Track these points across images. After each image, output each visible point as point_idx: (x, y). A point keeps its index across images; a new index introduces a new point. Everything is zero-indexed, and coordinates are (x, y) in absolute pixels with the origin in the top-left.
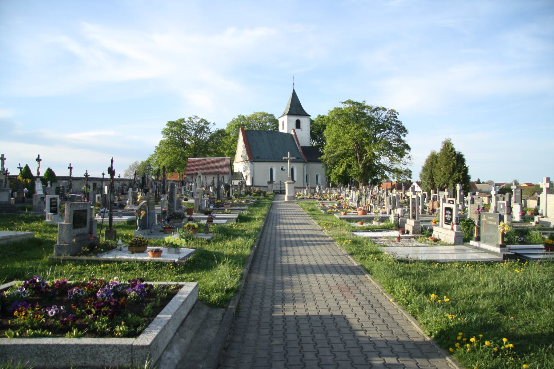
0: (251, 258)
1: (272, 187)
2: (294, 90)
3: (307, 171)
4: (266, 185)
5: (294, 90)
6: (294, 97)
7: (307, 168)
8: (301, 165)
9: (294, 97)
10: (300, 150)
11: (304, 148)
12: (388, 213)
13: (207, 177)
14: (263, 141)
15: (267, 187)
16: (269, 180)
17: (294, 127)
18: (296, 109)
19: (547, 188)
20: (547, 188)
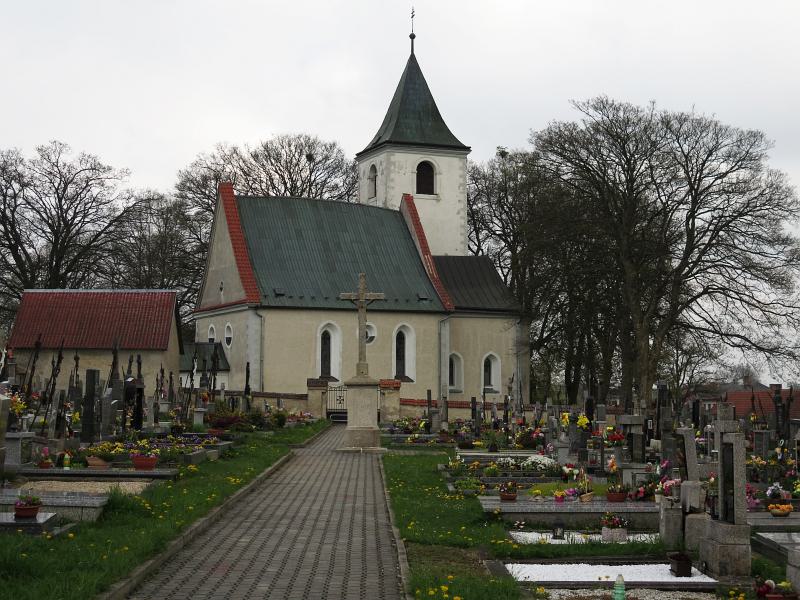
0: (405, 207)
1: (324, 400)
2: (413, 58)
3: (454, 344)
4: (304, 390)
5: (413, 58)
6: (413, 77)
7: (452, 333)
8: (430, 323)
9: (413, 77)
10: (430, 269)
11: (444, 263)
12: (452, 388)
13: (64, 355)
14: (299, 233)
15: (304, 397)
16: (317, 374)
17: (412, 189)
18: (414, 118)
19: (780, 386)
20: (780, 386)
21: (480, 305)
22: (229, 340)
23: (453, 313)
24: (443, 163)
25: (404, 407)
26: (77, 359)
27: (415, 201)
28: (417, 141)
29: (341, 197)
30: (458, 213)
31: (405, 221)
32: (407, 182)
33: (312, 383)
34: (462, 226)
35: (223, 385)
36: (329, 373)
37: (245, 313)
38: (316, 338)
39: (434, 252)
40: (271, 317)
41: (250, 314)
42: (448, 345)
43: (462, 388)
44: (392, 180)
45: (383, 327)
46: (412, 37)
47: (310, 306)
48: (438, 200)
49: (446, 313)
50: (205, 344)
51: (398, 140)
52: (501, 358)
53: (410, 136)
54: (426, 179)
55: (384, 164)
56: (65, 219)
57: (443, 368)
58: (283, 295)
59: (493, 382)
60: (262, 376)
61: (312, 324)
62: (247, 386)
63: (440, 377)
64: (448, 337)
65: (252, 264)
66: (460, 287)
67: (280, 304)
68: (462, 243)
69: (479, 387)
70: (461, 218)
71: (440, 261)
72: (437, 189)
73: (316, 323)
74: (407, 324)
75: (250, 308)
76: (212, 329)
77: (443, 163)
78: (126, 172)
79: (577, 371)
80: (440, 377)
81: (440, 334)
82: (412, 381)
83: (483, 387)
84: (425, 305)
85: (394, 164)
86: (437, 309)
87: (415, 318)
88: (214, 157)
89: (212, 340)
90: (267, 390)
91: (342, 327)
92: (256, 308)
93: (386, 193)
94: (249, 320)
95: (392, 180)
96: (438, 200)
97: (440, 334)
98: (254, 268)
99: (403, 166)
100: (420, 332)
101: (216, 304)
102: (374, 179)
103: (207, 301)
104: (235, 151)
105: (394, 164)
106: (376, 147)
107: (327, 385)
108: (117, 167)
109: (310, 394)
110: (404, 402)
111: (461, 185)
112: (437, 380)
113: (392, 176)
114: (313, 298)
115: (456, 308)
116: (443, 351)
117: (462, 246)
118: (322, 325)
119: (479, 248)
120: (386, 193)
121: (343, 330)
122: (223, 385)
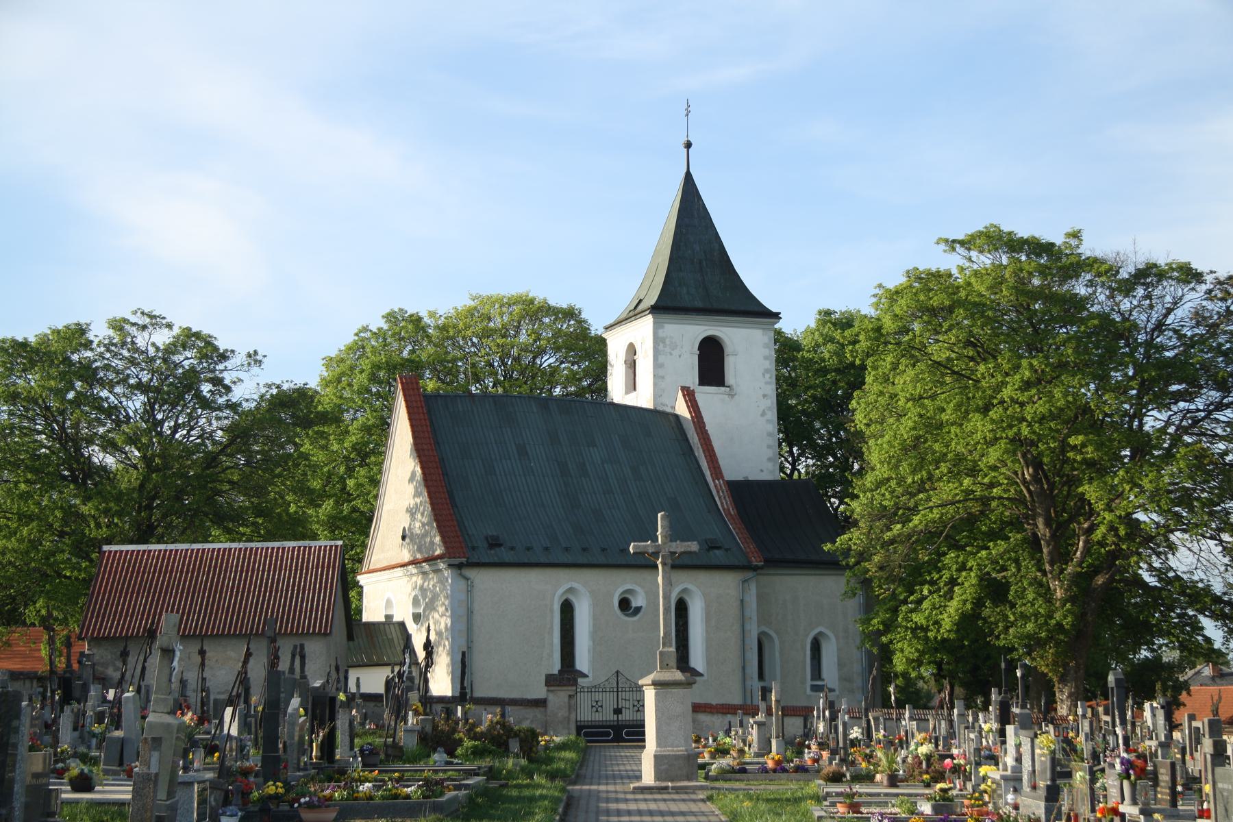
1: (572, 707)
3: (763, 618)
4: (540, 692)
5: (688, 177)
6: (692, 214)
7: (761, 598)
8: (726, 584)
9: (692, 214)
10: (723, 501)
11: (743, 491)
15: (540, 703)
16: (556, 667)
18: (699, 278)
23: (762, 568)
26: (202, 653)
27: (698, 397)
29: (581, 392)
30: (763, 414)
33: (551, 681)
34: (770, 434)
38: (552, 611)
39: (727, 478)
42: (755, 618)
46: (688, 145)
47: (542, 560)
48: (732, 396)
50: (378, 624)
52: (837, 638)
56: (160, 434)
57: (748, 655)
58: (500, 545)
59: (825, 674)
63: (744, 668)
64: (754, 606)
67: (496, 560)
68: (769, 459)
69: (803, 682)
70: (768, 421)
72: (730, 378)
74: (575, 585)
79: (292, 670)
80: (744, 668)
81: (742, 601)
82: (701, 675)
83: (809, 683)
85: (664, 343)
86: (737, 563)
87: (703, 577)
88: (764, 396)
91: (646, 593)
97: (742, 601)
100: (708, 595)
109: (551, 697)
112: (739, 675)
114: (547, 549)
115: (766, 561)
116: (747, 627)
117: (770, 465)
118: (561, 591)
119: (794, 469)
121: (590, 594)
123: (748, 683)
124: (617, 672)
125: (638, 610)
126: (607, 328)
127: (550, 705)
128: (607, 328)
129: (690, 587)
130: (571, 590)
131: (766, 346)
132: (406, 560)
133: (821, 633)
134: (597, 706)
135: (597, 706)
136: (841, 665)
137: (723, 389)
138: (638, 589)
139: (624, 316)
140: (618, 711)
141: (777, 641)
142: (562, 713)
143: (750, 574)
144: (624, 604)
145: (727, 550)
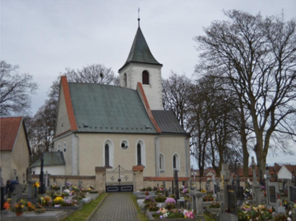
2: (139, 32)
4: (93, 174)
5: (139, 32)
6: (139, 36)
8: (151, 139)
9: (139, 36)
10: (150, 115)
12: (161, 170)
15: (93, 178)
21: (170, 131)
22: (65, 150)
24: (152, 71)
25: (145, 182)
28: (142, 61)
30: (159, 93)
31: (139, 94)
32: (139, 78)
33: (99, 170)
35: (47, 172)
36: (108, 164)
37: (70, 136)
40: (82, 137)
41: (73, 135)
43: (165, 170)
44: (133, 78)
45: (132, 141)
46: (139, 20)
48: (151, 87)
49: (158, 134)
51: (135, 60)
53: (139, 60)
54: (146, 77)
55: (130, 72)
60: (78, 167)
61: (99, 141)
62: (176, 172)
65: (75, 112)
66: (164, 124)
71: (154, 112)
73: (102, 140)
74: (109, 139)
75: (73, 132)
76: (65, 144)
77: (152, 71)
78: (17, 67)
81: (155, 145)
84: (149, 131)
87: (145, 137)
89: (59, 151)
90: (81, 174)
92: (75, 133)
93: (130, 84)
94: (73, 138)
95: (133, 78)
96: (151, 87)
97: (155, 145)
98: (75, 114)
99: (137, 72)
100: (147, 142)
101: (61, 133)
102: (125, 80)
103: (58, 133)
104: (73, 71)
105: (133, 71)
106: (127, 64)
107: (105, 171)
108: (13, 64)
110: (147, 179)
111: (159, 80)
112: (155, 166)
113: (133, 76)
116: (157, 152)
120: (130, 84)
121: (114, 142)
122: (47, 172)
123: (157, 169)
124: (119, 166)
125: (127, 147)
126: (125, 75)
127: (96, 178)
128: (125, 75)
129: (142, 140)
130: (108, 141)
131: (160, 102)
132: (263, 99)
133: (176, 154)
134: (112, 178)
135: (112, 178)
136: (181, 164)
137: (148, 85)
138: (127, 140)
139: (198, 161)
140: (119, 180)
141: (164, 157)
142: (101, 182)
143: (157, 136)
144: (123, 145)
145: (151, 129)
